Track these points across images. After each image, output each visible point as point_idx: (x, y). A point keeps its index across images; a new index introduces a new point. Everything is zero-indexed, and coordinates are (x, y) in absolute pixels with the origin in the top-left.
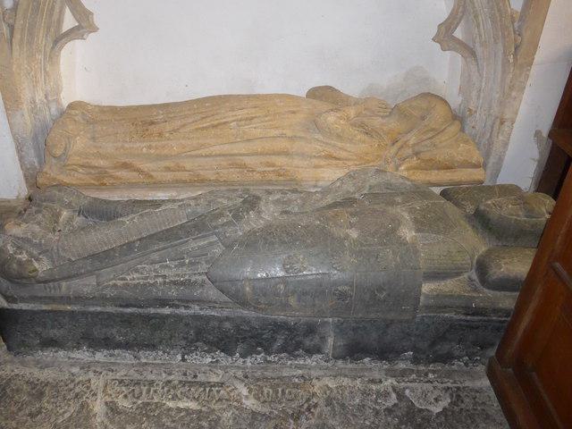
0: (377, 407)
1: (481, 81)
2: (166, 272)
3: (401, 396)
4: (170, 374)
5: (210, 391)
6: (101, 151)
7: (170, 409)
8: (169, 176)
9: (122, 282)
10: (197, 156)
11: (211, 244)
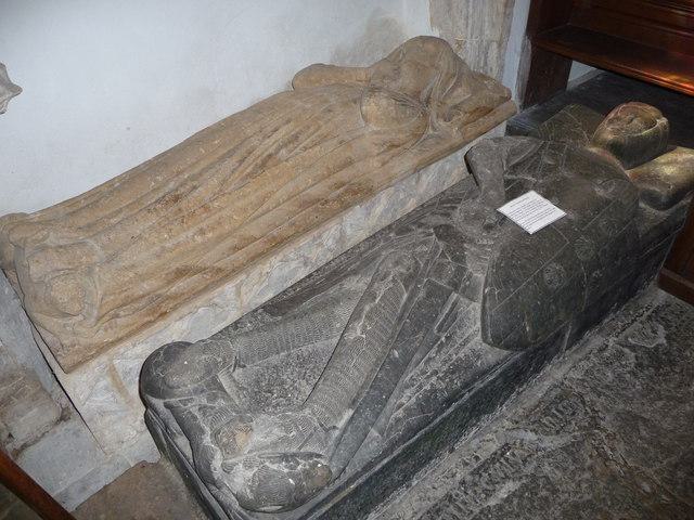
0: (628, 369)
1: (468, 6)
2: (434, 366)
3: (633, 348)
4: (454, 476)
5: (507, 460)
6: (140, 270)
7: (500, 507)
8: (240, 256)
9: (401, 411)
10: (258, 217)
11: (455, 304)
